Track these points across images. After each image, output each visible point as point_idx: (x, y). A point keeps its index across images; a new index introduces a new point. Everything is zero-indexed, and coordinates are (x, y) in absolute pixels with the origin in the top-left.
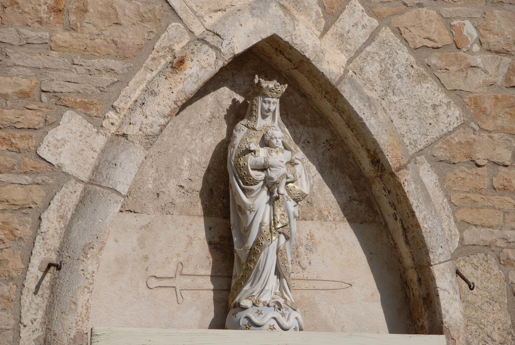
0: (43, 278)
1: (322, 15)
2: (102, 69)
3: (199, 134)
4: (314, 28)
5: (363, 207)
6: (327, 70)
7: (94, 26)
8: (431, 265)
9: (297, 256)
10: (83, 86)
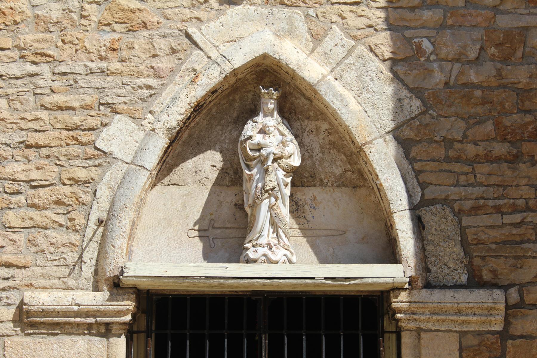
1: (310, 40)
2: (143, 86)
3: (228, 129)
4: (304, 49)
5: (355, 176)
6: (307, 76)
7: (139, 57)
8: (392, 214)
9: (303, 212)
10: (129, 98)
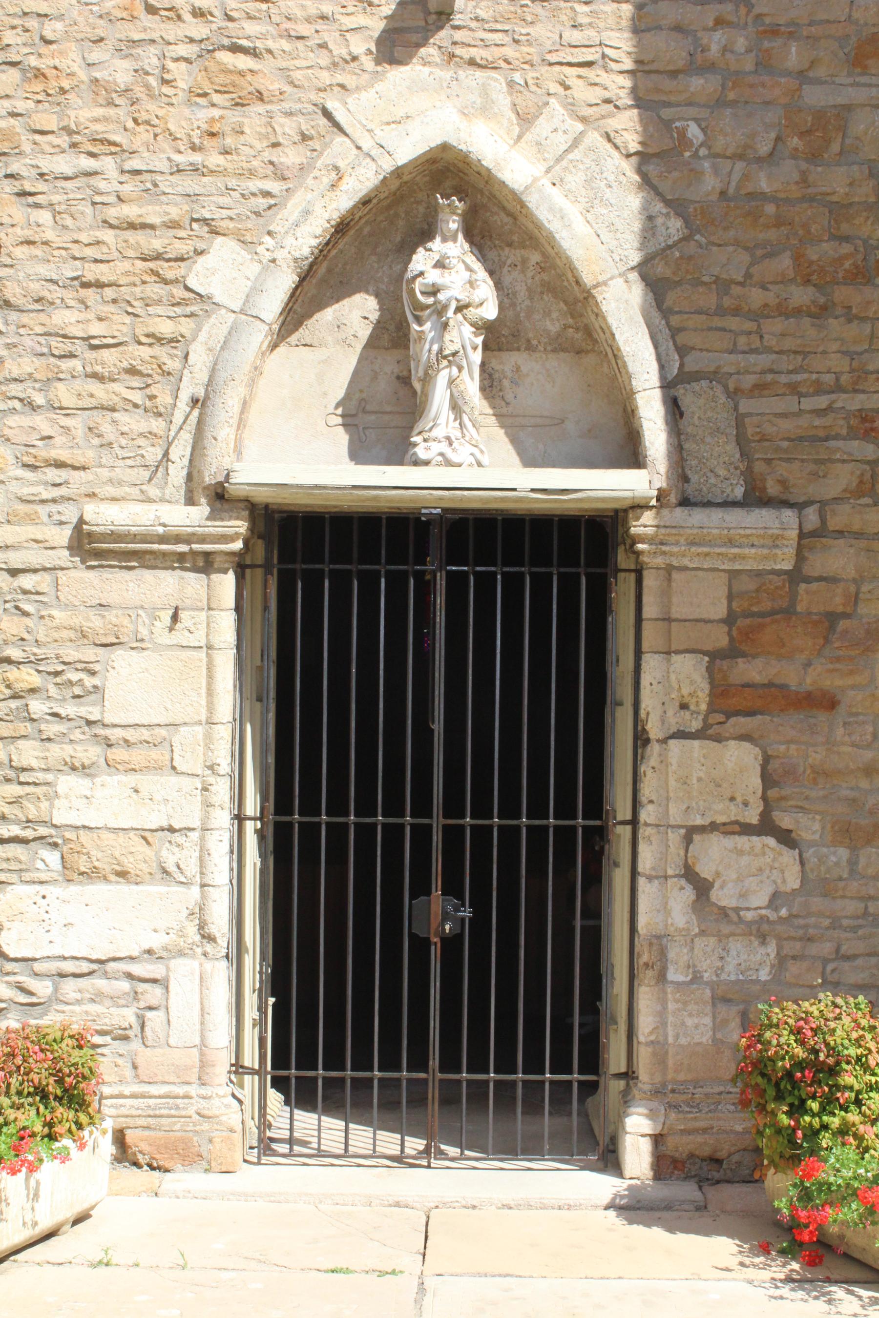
0: (190, 413)
10: (236, 211)
